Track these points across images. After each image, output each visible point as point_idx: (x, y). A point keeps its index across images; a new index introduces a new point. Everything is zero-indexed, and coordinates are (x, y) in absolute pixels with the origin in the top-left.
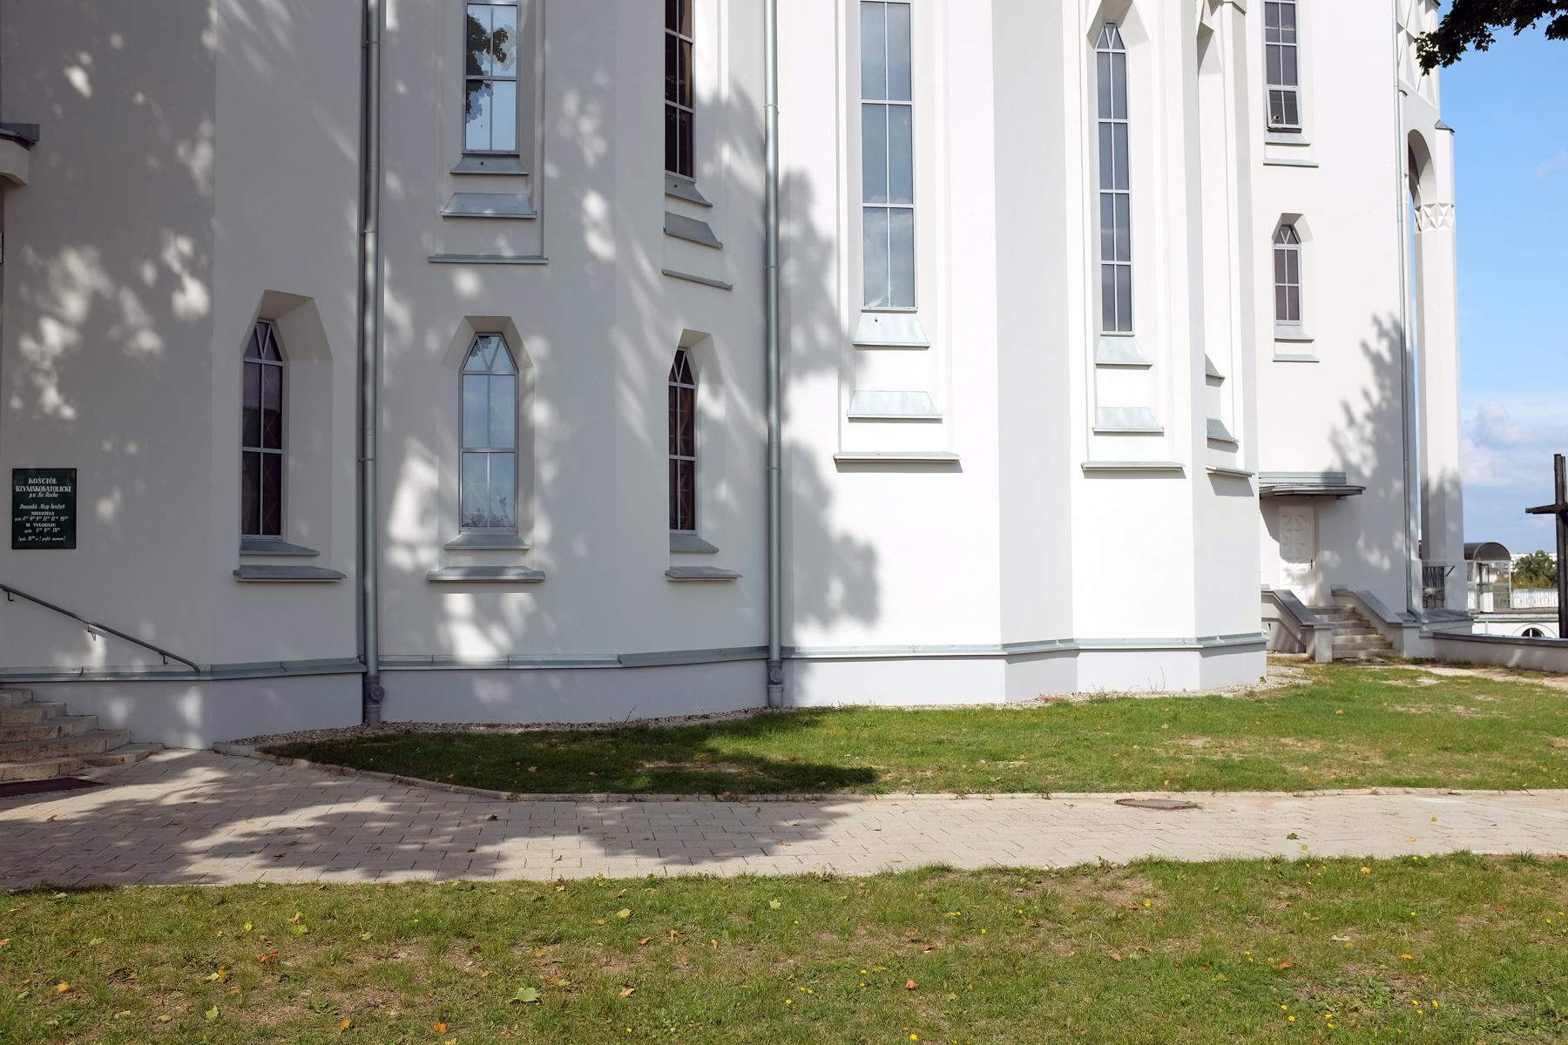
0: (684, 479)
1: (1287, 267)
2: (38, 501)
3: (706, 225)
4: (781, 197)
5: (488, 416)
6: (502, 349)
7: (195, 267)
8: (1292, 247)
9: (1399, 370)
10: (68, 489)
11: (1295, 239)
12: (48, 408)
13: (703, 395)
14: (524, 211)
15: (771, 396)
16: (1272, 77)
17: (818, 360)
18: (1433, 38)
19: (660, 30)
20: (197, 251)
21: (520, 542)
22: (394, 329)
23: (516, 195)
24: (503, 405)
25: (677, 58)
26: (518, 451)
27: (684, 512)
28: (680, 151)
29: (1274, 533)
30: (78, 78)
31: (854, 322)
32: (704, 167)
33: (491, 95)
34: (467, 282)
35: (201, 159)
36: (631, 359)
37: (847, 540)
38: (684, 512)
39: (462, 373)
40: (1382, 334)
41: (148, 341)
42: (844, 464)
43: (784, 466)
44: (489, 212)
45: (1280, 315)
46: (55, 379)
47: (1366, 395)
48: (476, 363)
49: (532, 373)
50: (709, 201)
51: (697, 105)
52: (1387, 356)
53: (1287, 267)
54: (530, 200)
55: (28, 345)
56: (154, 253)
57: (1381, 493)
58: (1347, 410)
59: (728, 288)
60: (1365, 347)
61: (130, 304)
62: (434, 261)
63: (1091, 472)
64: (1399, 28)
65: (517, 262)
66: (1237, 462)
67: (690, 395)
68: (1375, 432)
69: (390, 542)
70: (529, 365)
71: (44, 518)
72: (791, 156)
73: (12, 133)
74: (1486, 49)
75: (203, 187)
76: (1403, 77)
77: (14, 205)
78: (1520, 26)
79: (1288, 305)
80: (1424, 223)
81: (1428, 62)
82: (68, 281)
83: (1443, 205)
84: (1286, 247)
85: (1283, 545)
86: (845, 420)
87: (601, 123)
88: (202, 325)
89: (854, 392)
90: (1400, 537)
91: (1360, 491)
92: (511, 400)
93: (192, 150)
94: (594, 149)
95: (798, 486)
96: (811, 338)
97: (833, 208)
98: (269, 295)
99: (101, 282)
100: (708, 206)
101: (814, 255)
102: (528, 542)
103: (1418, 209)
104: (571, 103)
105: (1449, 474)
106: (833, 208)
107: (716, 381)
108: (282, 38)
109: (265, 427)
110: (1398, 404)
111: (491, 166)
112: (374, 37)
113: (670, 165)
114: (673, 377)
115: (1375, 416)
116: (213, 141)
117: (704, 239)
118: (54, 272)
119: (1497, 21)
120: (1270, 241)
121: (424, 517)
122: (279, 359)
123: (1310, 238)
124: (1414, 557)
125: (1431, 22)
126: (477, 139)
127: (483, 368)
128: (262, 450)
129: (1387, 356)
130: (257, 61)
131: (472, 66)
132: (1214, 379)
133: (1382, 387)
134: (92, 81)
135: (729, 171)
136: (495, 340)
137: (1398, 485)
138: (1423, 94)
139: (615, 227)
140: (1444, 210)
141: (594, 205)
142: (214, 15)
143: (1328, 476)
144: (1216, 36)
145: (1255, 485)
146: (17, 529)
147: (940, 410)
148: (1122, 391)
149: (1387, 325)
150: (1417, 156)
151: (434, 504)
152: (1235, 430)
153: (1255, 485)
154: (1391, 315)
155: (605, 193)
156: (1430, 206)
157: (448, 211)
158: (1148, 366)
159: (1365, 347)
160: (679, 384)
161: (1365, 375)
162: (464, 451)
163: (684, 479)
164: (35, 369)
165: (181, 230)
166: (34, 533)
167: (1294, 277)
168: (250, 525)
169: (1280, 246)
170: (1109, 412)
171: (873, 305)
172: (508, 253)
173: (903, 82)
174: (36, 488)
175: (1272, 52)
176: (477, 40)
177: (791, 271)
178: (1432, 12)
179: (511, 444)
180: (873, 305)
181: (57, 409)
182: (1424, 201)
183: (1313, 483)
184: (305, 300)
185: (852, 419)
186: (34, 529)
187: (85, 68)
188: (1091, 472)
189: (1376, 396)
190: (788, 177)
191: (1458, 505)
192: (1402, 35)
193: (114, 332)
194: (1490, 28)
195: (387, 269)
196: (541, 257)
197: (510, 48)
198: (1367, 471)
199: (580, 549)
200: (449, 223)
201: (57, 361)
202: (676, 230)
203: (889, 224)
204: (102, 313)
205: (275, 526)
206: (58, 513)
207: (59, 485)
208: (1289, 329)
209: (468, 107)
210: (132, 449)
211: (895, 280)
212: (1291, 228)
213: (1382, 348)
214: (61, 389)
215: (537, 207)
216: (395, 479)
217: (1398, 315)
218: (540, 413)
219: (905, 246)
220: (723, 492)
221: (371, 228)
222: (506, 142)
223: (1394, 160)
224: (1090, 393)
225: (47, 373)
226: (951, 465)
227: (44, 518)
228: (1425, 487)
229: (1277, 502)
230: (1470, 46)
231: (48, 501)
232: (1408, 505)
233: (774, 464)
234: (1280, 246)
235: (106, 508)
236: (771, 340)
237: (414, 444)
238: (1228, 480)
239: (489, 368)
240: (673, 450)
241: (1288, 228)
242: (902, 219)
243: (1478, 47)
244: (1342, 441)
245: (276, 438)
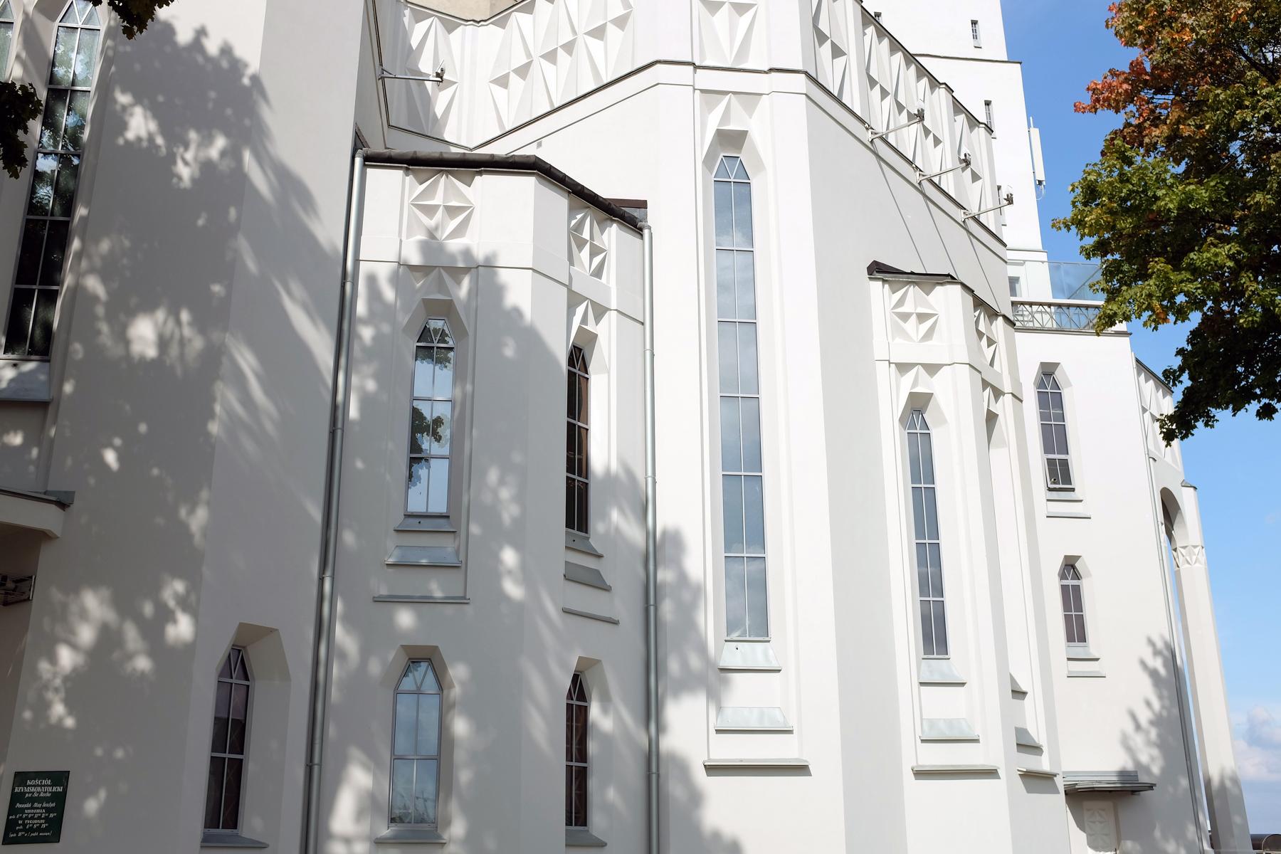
0: (578, 781)
1: (1072, 599)
2: (32, 800)
3: (597, 572)
4: (659, 549)
5: (417, 726)
6: (430, 675)
7: (185, 604)
8: (1075, 582)
9: (1173, 682)
10: (60, 789)
11: (1077, 576)
12: (53, 719)
13: (595, 712)
14: (452, 560)
15: (651, 711)
16: (1048, 448)
17: (689, 683)
18: (1171, 418)
19: (562, 418)
20: (188, 592)
21: (440, 837)
22: (343, 656)
23: (445, 548)
24: (430, 717)
25: (576, 440)
26: (440, 758)
27: (577, 811)
28: (578, 511)
29: (1081, 825)
30: (110, 457)
31: (719, 650)
32: (597, 526)
33: (429, 468)
34: (405, 618)
35: (198, 519)
36: (537, 683)
37: (717, 836)
38: (577, 811)
39: (397, 692)
40: (1157, 653)
41: (143, 663)
42: (712, 769)
43: (662, 771)
44: (424, 561)
45: (1070, 638)
46: (62, 695)
47: (1148, 704)
48: (408, 683)
49: (456, 692)
50: (600, 551)
51: (591, 477)
52: (1162, 671)
53: (1072, 599)
54: (457, 552)
55: (44, 666)
56: (154, 591)
57: (1171, 789)
58: (1134, 717)
59: (616, 623)
60: (1143, 664)
61: (132, 635)
62: (378, 600)
63: (920, 774)
64: (1144, 410)
65: (446, 601)
66: (1044, 764)
67: (584, 711)
68: (1159, 735)
69: (330, 836)
70: (451, 686)
71: (35, 815)
72: (667, 516)
73: (53, 498)
74: (1212, 426)
75: (198, 538)
76: (1151, 447)
77: (47, 557)
78: (1236, 410)
79: (1076, 630)
80: (1181, 561)
81: (1169, 437)
82: (84, 615)
83: (1195, 547)
84: (1070, 582)
85: (1089, 836)
86: (712, 731)
87: (517, 493)
88: (188, 650)
89: (719, 709)
90: (1191, 829)
91: (1151, 787)
92: (436, 714)
93: (192, 511)
94: (510, 512)
95: (674, 789)
96: (685, 664)
97: (701, 559)
98: (243, 627)
99: (110, 616)
100: (600, 556)
101: (686, 596)
102: (446, 836)
103: (1175, 550)
104: (493, 476)
105: (1228, 772)
106: (701, 559)
107: (606, 699)
108: (269, 427)
109: (231, 734)
110: (1176, 711)
111: (427, 525)
112: (340, 425)
113: (569, 524)
114: (570, 696)
115: (1157, 722)
116: (208, 503)
117: (597, 583)
118: (74, 608)
119: (1218, 406)
120: (1057, 578)
121: (360, 815)
122: (247, 679)
123: (1089, 575)
124: (1206, 847)
125: (1167, 405)
126: (417, 503)
127: (414, 688)
128: (227, 755)
129: (1162, 671)
130: (249, 445)
131: (415, 447)
132: (1019, 694)
133: (1161, 697)
134: (120, 459)
135: (617, 530)
136: (424, 665)
137: (1184, 782)
138: (1168, 459)
139: (526, 575)
140: (1196, 550)
141: (509, 557)
142: (218, 408)
143: (1123, 774)
144: (1001, 419)
145: (1060, 783)
146: (10, 826)
147: (792, 723)
148: (944, 707)
149: (1160, 645)
150: (1169, 509)
151: (369, 805)
152: (1040, 737)
153: (1060, 783)
154: (1162, 637)
155: (518, 547)
156: (1184, 547)
157: (391, 561)
158: (963, 684)
159: (1143, 664)
160: (575, 702)
161: (1145, 688)
162: (395, 758)
163: (578, 781)
164: (46, 687)
165: (177, 574)
166: (24, 830)
167: (1079, 607)
168: (212, 820)
169: (1065, 582)
170: (932, 723)
171: (734, 636)
172: (438, 594)
173: (756, 459)
174: (33, 789)
175: (1046, 430)
176: (419, 424)
177: (667, 609)
178: (1168, 398)
179: (433, 751)
180: (734, 636)
181: (61, 720)
182: (1179, 544)
183: (1111, 781)
184: (271, 631)
185: (718, 731)
186: (24, 825)
187: (116, 449)
188: (920, 774)
189: (1156, 705)
190: (664, 533)
191: (1240, 799)
192: (1147, 415)
193: (116, 655)
194: (1213, 411)
195: (340, 606)
196: (464, 598)
197: (445, 431)
198: (1156, 770)
199: (490, 844)
200: (391, 570)
201: (66, 679)
202: (573, 576)
203: (746, 567)
204: (108, 638)
205: (232, 822)
206: (48, 810)
207: (52, 786)
208: (1078, 650)
209: (411, 476)
210: (119, 754)
211: (752, 618)
212: (1073, 567)
213: (1158, 664)
214: (68, 702)
215: (462, 557)
216: (337, 782)
217: (1167, 637)
218: (460, 727)
219: (760, 585)
220: (612, 794)
221: (328, 573)
222: (439, 506)
223: (1152, 512)
224: (917, 708)
225: (56, 690)
226: (800, 769)
227: (35, 815)
228: (1208, 783)
229: (1083, 798)
230: (1200, 424)
231: (40, 800)
232: (1195, 800)
233: (654, 769)
234: (1065, 582)
235: (92, 806)
236: (651, 666)
237: (355, 752)
238: (1036, 780)
239: (419, 688)
240: (569, 757)
241: (1070, 567)
242: (756, 565)
243: (1206, 425)
244: (1131, 743)
245: (239, 746)
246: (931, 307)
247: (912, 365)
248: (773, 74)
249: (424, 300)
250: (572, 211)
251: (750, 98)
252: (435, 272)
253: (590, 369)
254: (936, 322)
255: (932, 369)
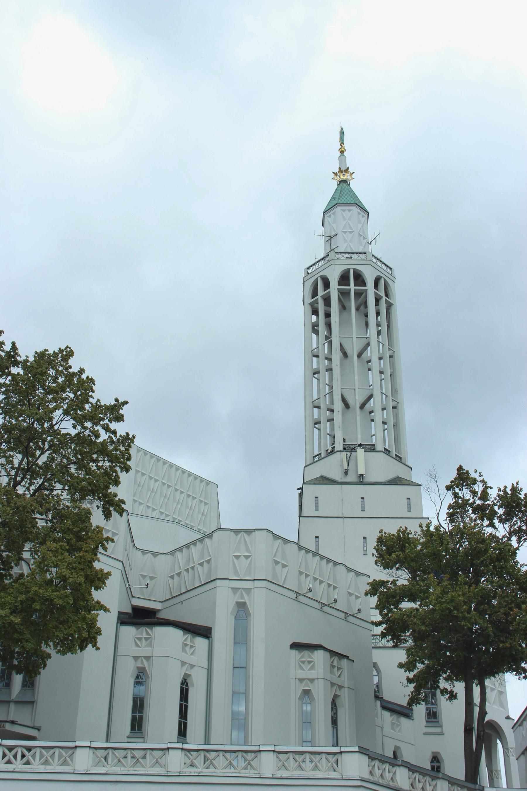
8: (438, 764)
84: (436, 764)
120: (429, 763)
169: (433, 764)
234: (433, 764)
246: (312, 658)
247: (304, 679)
248: (255, 581)
249: (303, 690)
250: (331, 657)
251: (248, 590)
252: (305, 681)
253: (337, 706)
254: (151, 641)
255: (312, 680)
